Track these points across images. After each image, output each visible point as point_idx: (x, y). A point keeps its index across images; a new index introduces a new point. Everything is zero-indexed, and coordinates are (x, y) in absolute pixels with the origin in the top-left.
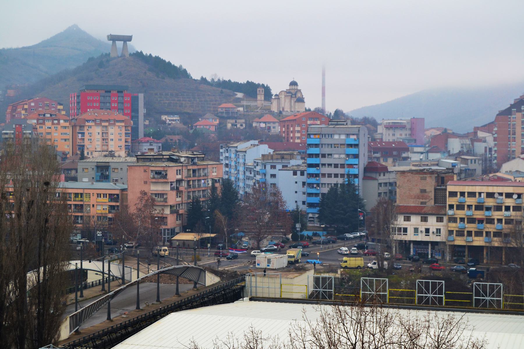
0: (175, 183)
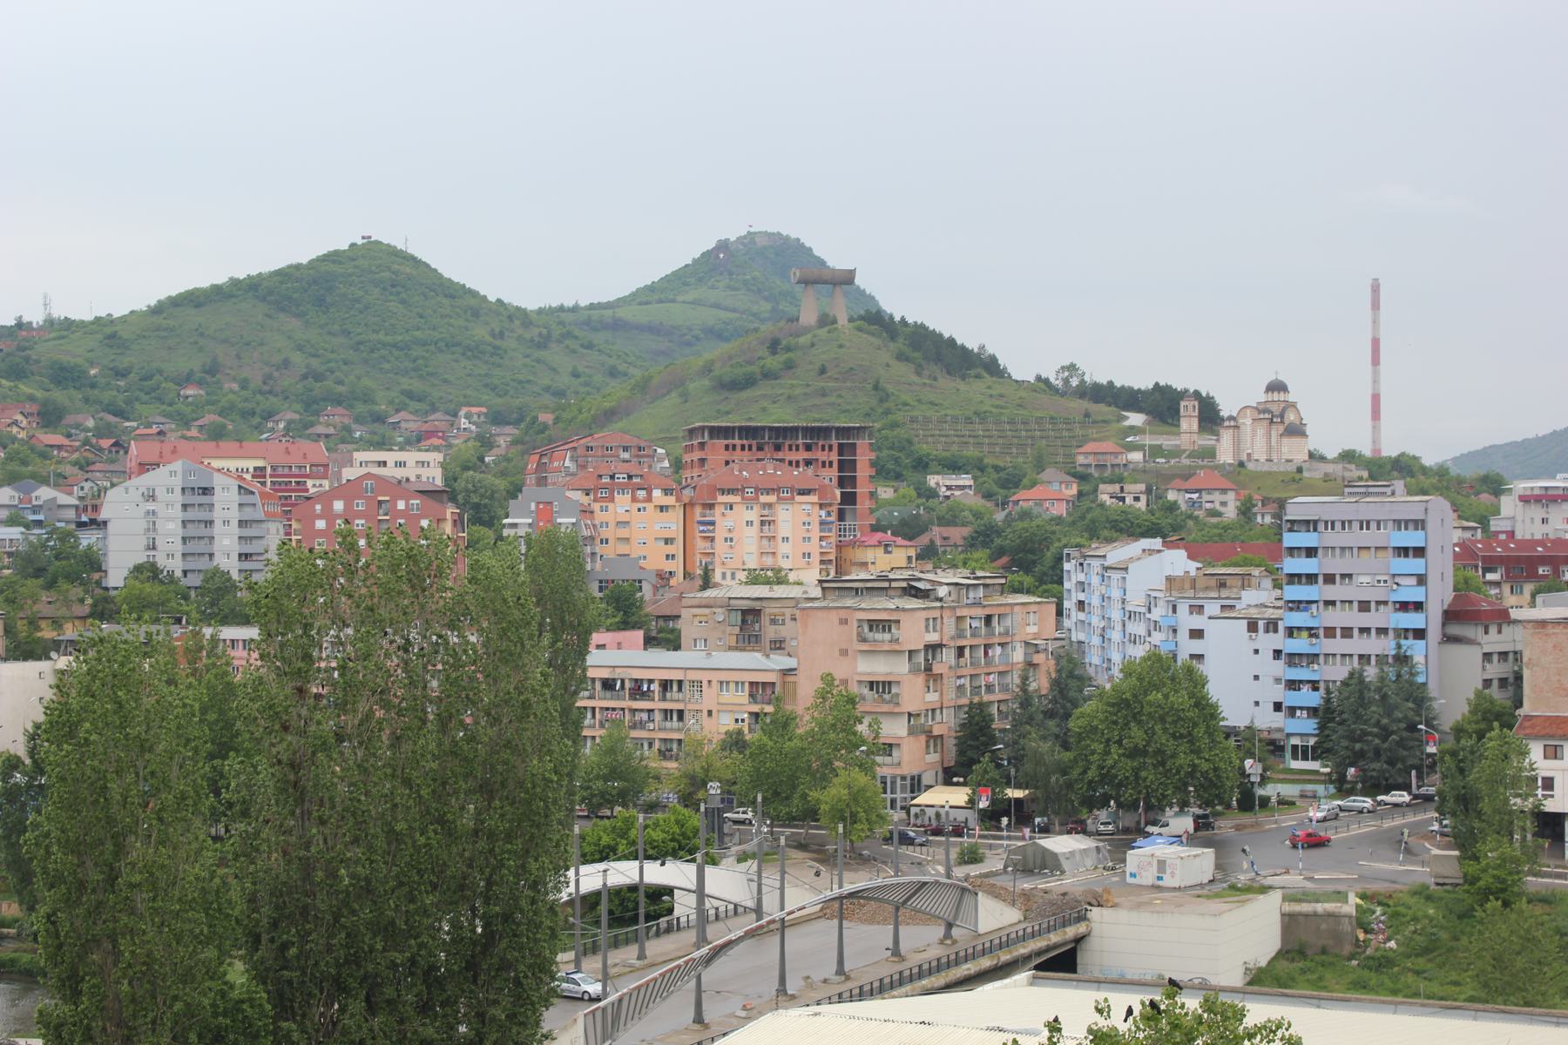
0: (922, 654)
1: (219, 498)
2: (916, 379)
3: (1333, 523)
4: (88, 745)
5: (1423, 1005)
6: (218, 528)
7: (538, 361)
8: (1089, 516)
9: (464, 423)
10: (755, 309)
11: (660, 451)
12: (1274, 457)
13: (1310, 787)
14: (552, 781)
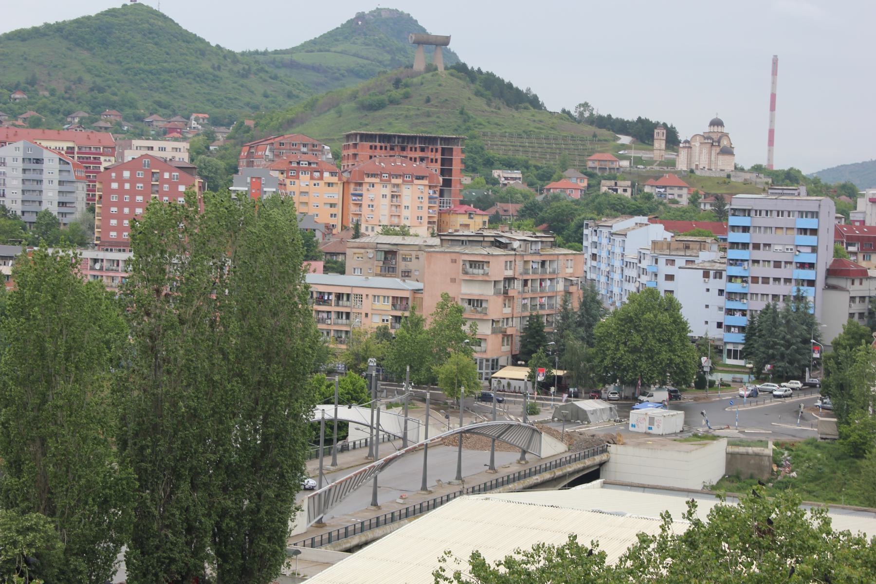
1: (46, 165)
2: (486, 108)
3: (760, 211)
4: (35, 320)
5: (843, 508)
6: (45, 185)
7: (242, 86)
8: (597, 201)
9: (194, 124)
10: (380, 58)
11: (326, 147)
12: (713, 167)
13: (738, 376)
14: (308, 354)
